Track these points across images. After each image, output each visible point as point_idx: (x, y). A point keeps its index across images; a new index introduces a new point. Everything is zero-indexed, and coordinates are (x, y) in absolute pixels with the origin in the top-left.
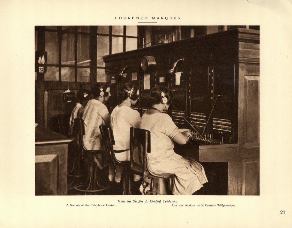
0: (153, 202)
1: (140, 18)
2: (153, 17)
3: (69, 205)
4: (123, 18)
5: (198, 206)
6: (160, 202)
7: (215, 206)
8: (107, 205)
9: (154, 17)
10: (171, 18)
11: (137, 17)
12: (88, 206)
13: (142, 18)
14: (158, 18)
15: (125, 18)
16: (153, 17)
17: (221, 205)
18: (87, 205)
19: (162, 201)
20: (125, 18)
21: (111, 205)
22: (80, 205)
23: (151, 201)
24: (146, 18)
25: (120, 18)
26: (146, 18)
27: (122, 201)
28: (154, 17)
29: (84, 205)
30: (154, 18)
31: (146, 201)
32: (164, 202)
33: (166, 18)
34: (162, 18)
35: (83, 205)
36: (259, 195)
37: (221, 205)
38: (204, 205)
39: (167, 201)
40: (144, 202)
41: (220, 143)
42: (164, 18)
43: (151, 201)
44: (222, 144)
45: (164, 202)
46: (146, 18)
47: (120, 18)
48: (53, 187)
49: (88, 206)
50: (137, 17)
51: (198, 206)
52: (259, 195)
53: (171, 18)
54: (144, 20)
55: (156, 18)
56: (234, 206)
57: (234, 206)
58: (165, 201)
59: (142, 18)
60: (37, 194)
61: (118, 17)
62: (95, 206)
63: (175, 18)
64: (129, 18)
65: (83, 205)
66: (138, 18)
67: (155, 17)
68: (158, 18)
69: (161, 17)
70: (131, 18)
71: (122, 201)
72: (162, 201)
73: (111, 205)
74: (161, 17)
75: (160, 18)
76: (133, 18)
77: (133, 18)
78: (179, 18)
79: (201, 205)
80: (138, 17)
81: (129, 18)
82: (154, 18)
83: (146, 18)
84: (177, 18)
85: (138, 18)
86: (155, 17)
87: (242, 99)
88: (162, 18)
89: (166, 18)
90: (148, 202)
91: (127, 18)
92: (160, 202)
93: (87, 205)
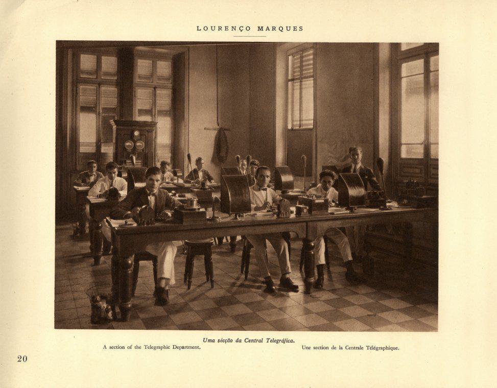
0: (249, 341)
1: (237, 28)
2: (259, 27)
3: (108, 347)
4: (210, 28)
5: (334, 348)
6: (261, 341)
7: (362, 348)
8: (347, 348)
10: (213, 28)
11: (233, 27)
13: (241, 28)
14: (268, 29)
16: (259, 27)
17: (373, 348)
18: (137, 347)
19: (265, 341)
21: (354, 348)
22: (126, 348)
23: (247, 340)
24: (248, 28)
25: (206, 29)
26: (248, 29)
27: (210, 341)
29: (133, 347)
30: (260, 29)
31: (238, 341)
32: (268, 342)
33: (281, 29)
35: (130, 348)
36: (56, 327)
38: (344, 348)
39: (273, 341)
40: (234, 341)
42: (277, 29)
43: (247, 340)
45: (268, 342)
46: (248, 29)
47: (206, 29)
50: (233, 27)
51: (334, 348)
52: (56, 327)
54: (245, 32)
55: (265, 28)
56: (396, 348)
57: (396, 348)
58: (269, 340)
59: (241, 28)
62: (151, 348)
64: (220, 28)
65: (130, 348)
66: (234, 28)
67: (262, 27)
68: (268, 29)
70: (223, 28)
71: (210, 341)
72: (265, 341)
73: (354, 348)
77: (226, 28)
79: (338, 348)
81: (220, 28)
82: (260, 29)
83: (248, 28)
85: (234, 28)
86: (262, 27)
88: (274, 29)
89: (281, 29)
90: (240, 341)
91: (217, 28)
92: (261, 341)
93: (137, 347)
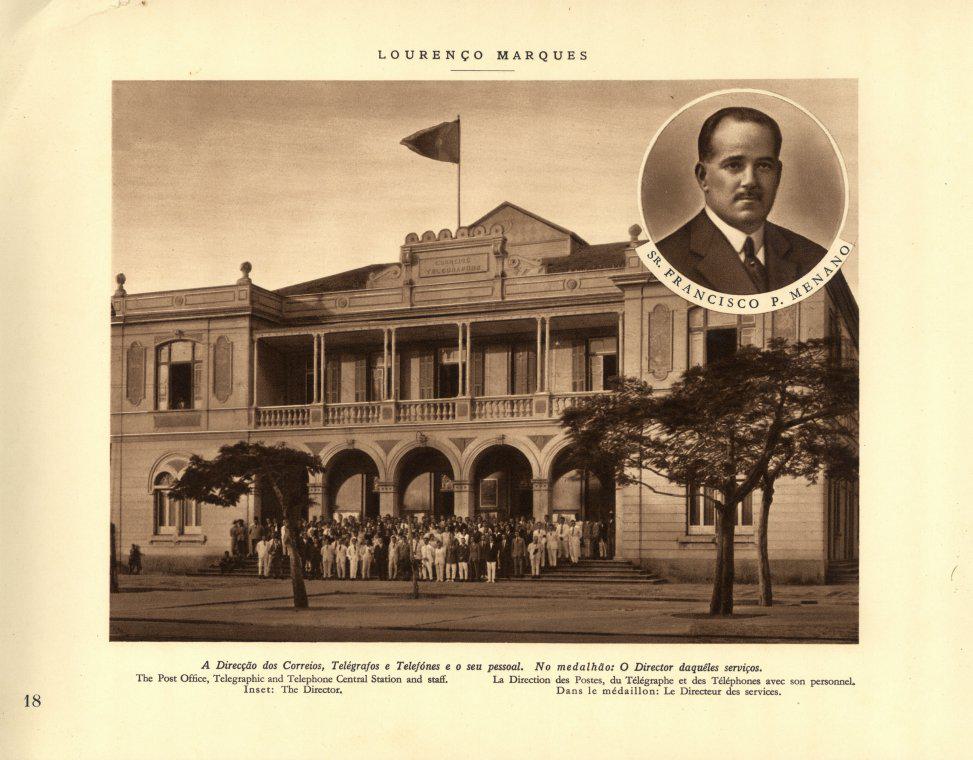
1: (457, 55)
2: (500, 53)
4: (403, 55)
11: (448, 52)
13: (465, 55)
15: (409, 55)
16: (500, 53)
20: (410, 55)
23: (287, 665)
24: (478, 55)
25: (395, 55)
26: (479, 55)
30: (503, 55)
33: (543, 56)
34: (529, 55)
42: (536, 56)
47: (395, 55)
50: (448, 52)
53: (557, 56)
55: (511, 55)
56: (849, 682)
58: (338, 665)
59: (465, 55)
61: (386, 53)
63: (423, 55)
66: (450, 54)
75: (523, 55)
76: (436, 55)
78: (584, 56)
80: (451, 50)
82: (503, 55)
84: (577, 55)
85: (450, 54)
88: (529, 55)
89: (543, 56)
91: (417, 55)
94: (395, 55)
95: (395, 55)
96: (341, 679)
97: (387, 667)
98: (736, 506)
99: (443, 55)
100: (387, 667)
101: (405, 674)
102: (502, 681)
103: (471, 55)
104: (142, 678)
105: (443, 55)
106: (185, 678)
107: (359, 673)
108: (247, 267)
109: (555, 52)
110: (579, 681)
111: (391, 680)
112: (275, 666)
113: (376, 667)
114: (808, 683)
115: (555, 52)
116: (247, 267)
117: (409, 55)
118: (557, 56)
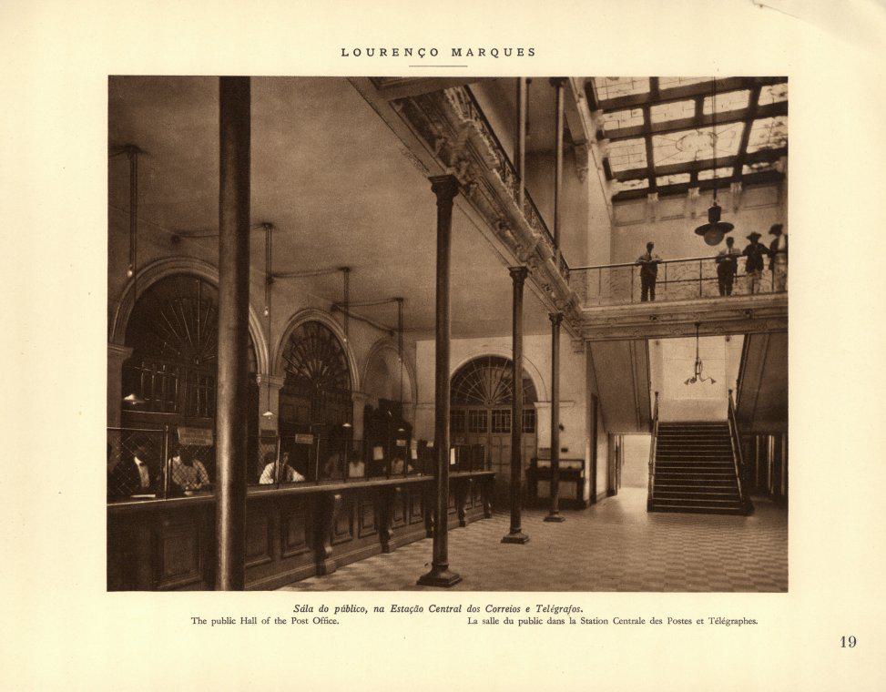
0: (437, 610)
1: (415, 52)
2: (454, 50)
4: (364, 52)
6: (458, 610)
8: (617, 621)
9: (457, 51)
11: (406, 50)
12: (283, 622)
13: (422, 52)
14: (470, 53)
15: (370, 53)
16: (454, 50)
17: (720, 621)
20: (371, 53)
21: (628, 622)
23: (489, 609)
24: (434, 52)
25: (357, 53)
26: (434, 52)
28: (457, 51)
29: (272, 621)
30: (457, 52)
31: (379, 610)
33: (495, 52)
34: (482, 52)
35: (267, 621)
37: (720, 621)
41: (349, 428)
42: (488, 52)
43: (489, 609)
44: (351, 423)
46: (434, 52)
47: (357, 53)
48: (145, 571)
49: (283, 622)
50: (406, 50)
51: (700, 622)
53: (508, 53)
55: (464, 52)
56: (754, 622)
58: (542, 608)
59: (422, 52)
60: (112, 586)
61: (349, 51)
63: (520, 52)
65: (267, 621)
66: (408, 52)
67: (459, 50)
68: (470, 53)
69: (519, 49)
70: (390, 52)
73: (628, 622)
74: (519, 49)
75: (476, 52)
76: (395, 53)
77: (395, 53)
78: (532, 53)
80: (409, 48)
81: (383, 52)
82: (457, 52)
83: (434, 52)
84: (526, 52)
85: (408, 52)
87: (507, 292)
88: (482, 52)
89: (495, 52)
91: (377, 52)
94: (357, 52)
95: (357, 52)
96: (617, 621)
97: (527, 610)
98: (456, 460)
99: (402, 52)
100: (527, 610)
101: (544, 616)
102: (476, 622)
103: (428, 52)
104: (197, 621)
105: (402, 52)
106: (317, 620)
107: (562, 615)
108: (650, 246)
109: (368, 50)
110: (671, 623)
111: (329, 622)
112: (477, 610)
113: (518, 610)
114: (209, 622)
115: (368, 50)
116: (650, 246)
117: (370, 53)
118: (508, 53)
